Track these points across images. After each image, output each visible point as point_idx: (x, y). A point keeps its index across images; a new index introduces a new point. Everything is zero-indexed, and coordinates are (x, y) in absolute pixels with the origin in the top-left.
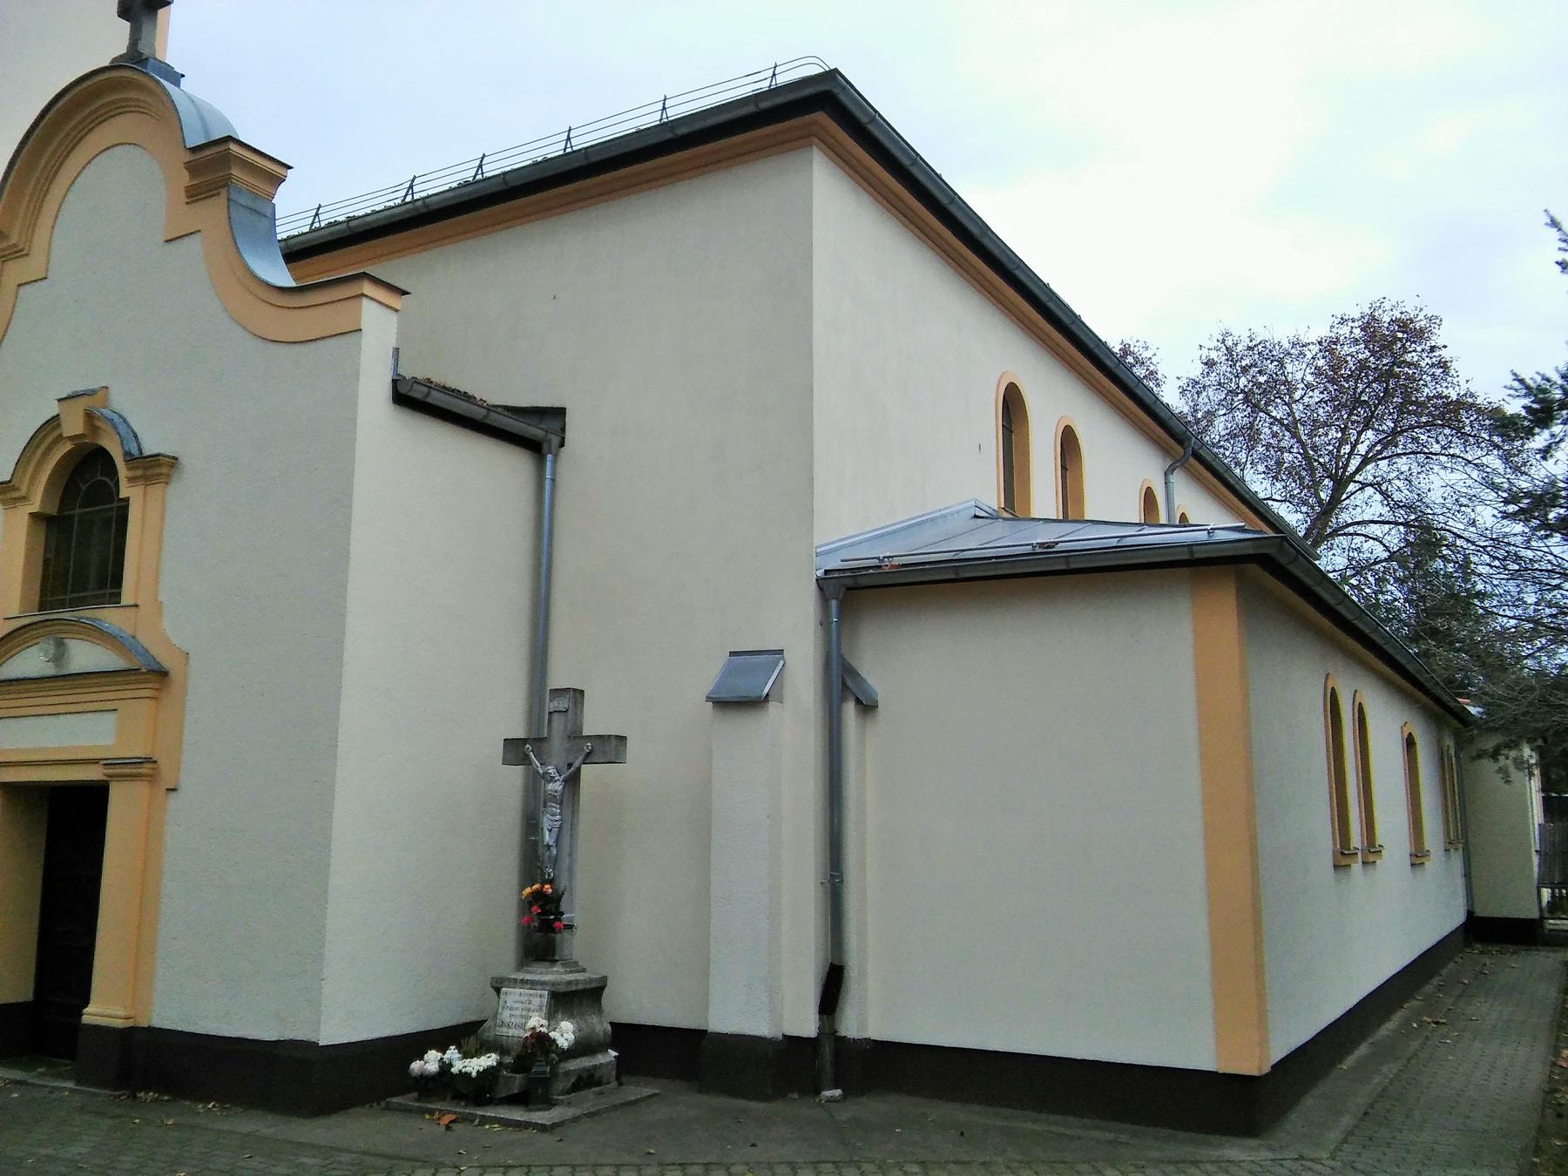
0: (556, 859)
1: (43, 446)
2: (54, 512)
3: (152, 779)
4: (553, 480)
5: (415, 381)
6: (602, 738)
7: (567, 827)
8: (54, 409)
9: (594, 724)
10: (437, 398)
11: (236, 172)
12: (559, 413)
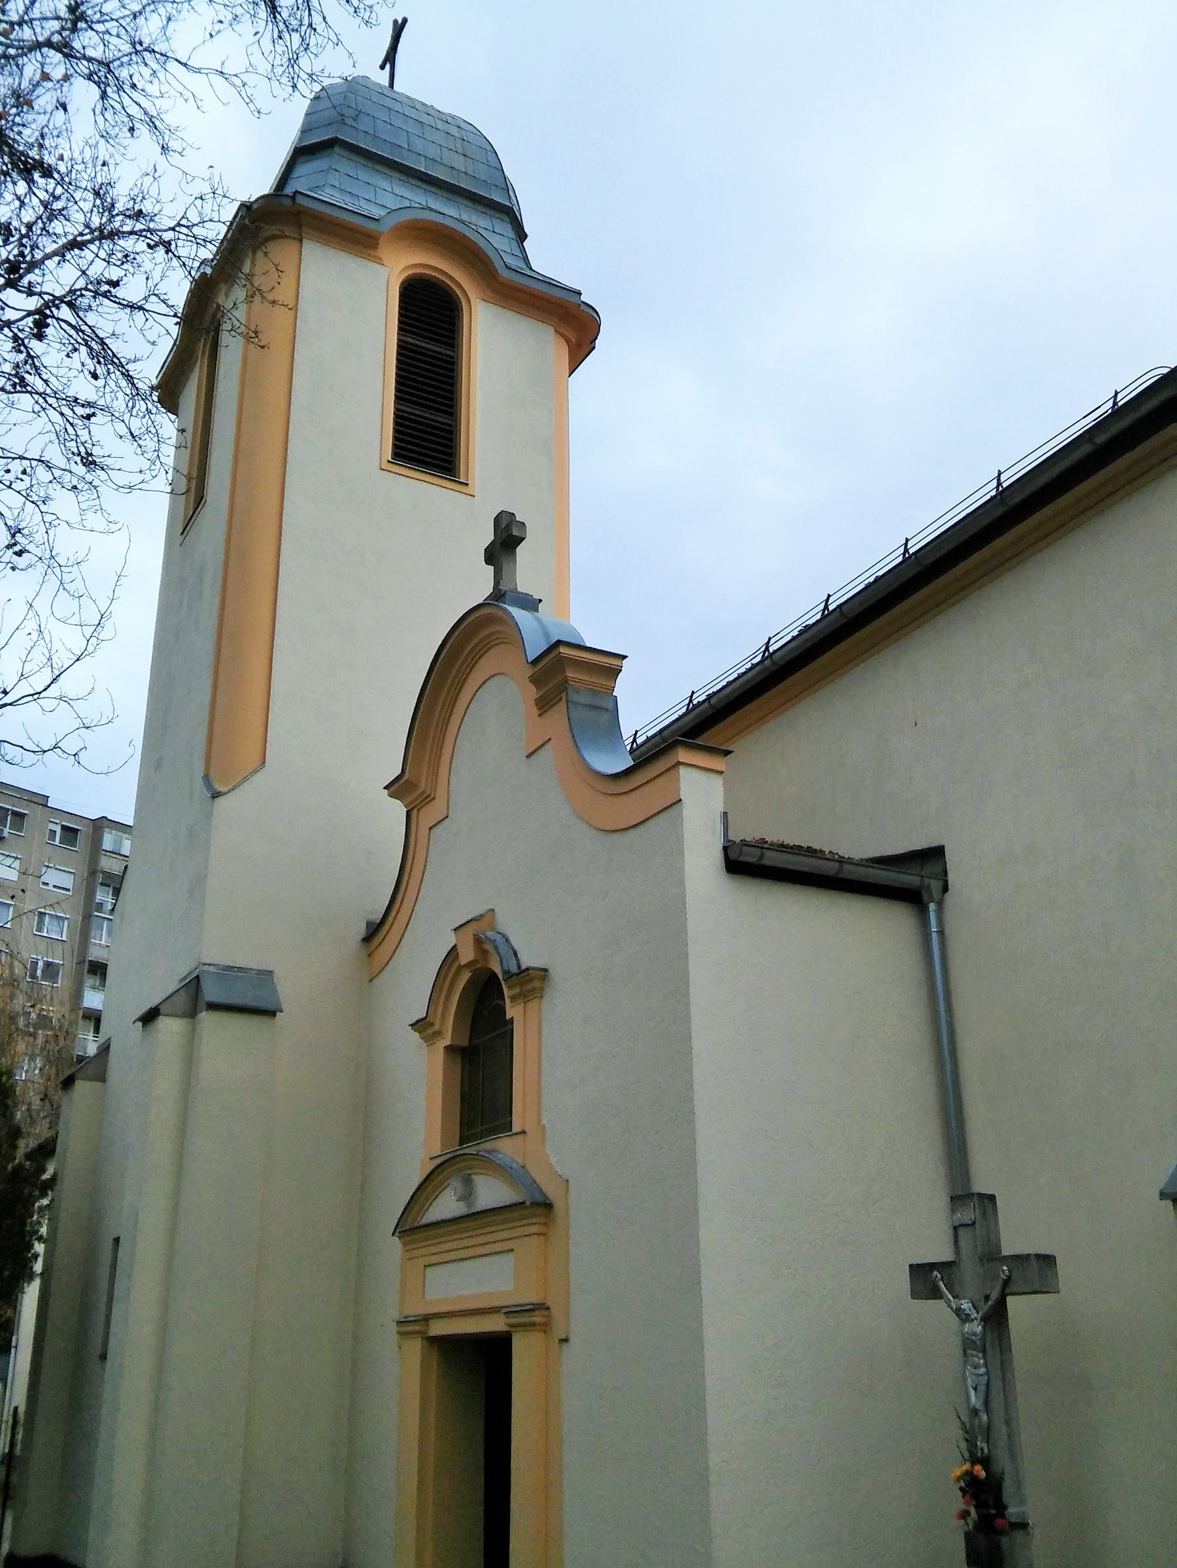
0: (989, 1428)
1: (449, 979)
3: (545, 1327)
4: (941, 933)
5: (744, 843)
6: (1020, 1260)
7: (997, 1385)
8: (451, 940)
9: (1015, 1239)
10: (773, 859)
12: (936, 854)
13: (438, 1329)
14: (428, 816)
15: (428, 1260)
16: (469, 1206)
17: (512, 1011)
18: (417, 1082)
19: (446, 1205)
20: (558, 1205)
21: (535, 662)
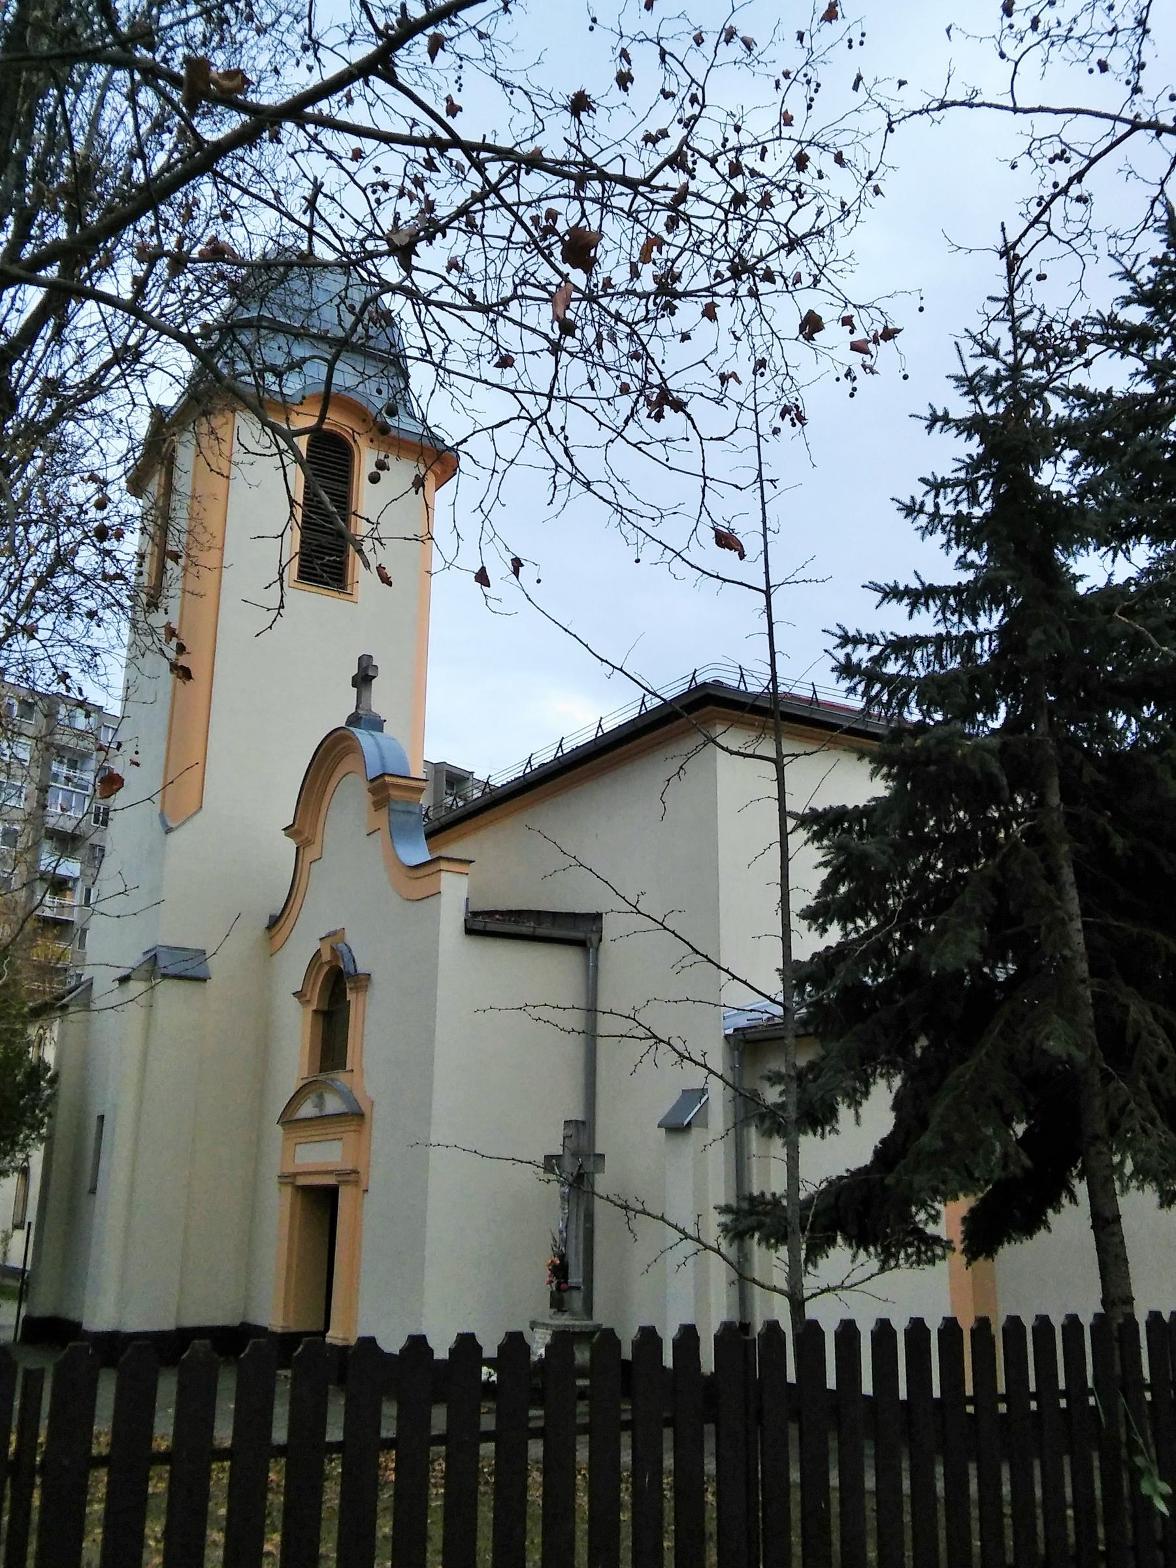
2: (326, 1008)
3: (356, 1183)
11: (394, 793)
13: (302, 1181)
14: (310, 854)
15: (299, 1140)
16: (321, 1110)
17: (350, 996)
18: (295, 1028)
19: (307, 1110)
20: (367, 1115)
21: (372, 780)
